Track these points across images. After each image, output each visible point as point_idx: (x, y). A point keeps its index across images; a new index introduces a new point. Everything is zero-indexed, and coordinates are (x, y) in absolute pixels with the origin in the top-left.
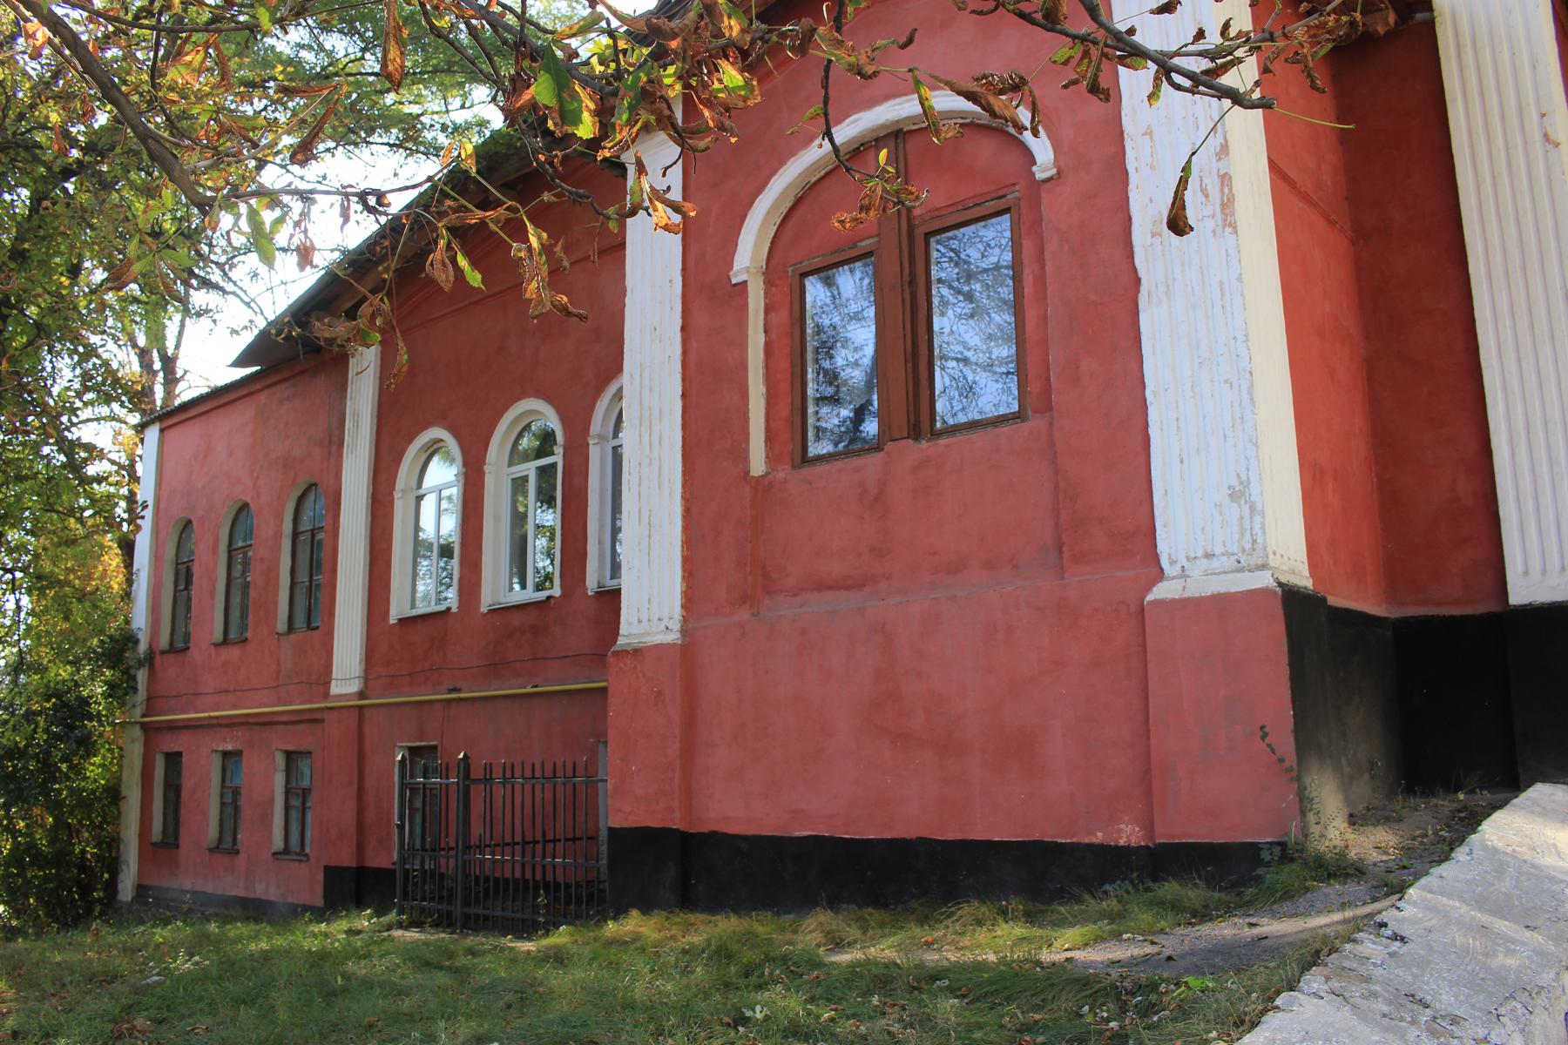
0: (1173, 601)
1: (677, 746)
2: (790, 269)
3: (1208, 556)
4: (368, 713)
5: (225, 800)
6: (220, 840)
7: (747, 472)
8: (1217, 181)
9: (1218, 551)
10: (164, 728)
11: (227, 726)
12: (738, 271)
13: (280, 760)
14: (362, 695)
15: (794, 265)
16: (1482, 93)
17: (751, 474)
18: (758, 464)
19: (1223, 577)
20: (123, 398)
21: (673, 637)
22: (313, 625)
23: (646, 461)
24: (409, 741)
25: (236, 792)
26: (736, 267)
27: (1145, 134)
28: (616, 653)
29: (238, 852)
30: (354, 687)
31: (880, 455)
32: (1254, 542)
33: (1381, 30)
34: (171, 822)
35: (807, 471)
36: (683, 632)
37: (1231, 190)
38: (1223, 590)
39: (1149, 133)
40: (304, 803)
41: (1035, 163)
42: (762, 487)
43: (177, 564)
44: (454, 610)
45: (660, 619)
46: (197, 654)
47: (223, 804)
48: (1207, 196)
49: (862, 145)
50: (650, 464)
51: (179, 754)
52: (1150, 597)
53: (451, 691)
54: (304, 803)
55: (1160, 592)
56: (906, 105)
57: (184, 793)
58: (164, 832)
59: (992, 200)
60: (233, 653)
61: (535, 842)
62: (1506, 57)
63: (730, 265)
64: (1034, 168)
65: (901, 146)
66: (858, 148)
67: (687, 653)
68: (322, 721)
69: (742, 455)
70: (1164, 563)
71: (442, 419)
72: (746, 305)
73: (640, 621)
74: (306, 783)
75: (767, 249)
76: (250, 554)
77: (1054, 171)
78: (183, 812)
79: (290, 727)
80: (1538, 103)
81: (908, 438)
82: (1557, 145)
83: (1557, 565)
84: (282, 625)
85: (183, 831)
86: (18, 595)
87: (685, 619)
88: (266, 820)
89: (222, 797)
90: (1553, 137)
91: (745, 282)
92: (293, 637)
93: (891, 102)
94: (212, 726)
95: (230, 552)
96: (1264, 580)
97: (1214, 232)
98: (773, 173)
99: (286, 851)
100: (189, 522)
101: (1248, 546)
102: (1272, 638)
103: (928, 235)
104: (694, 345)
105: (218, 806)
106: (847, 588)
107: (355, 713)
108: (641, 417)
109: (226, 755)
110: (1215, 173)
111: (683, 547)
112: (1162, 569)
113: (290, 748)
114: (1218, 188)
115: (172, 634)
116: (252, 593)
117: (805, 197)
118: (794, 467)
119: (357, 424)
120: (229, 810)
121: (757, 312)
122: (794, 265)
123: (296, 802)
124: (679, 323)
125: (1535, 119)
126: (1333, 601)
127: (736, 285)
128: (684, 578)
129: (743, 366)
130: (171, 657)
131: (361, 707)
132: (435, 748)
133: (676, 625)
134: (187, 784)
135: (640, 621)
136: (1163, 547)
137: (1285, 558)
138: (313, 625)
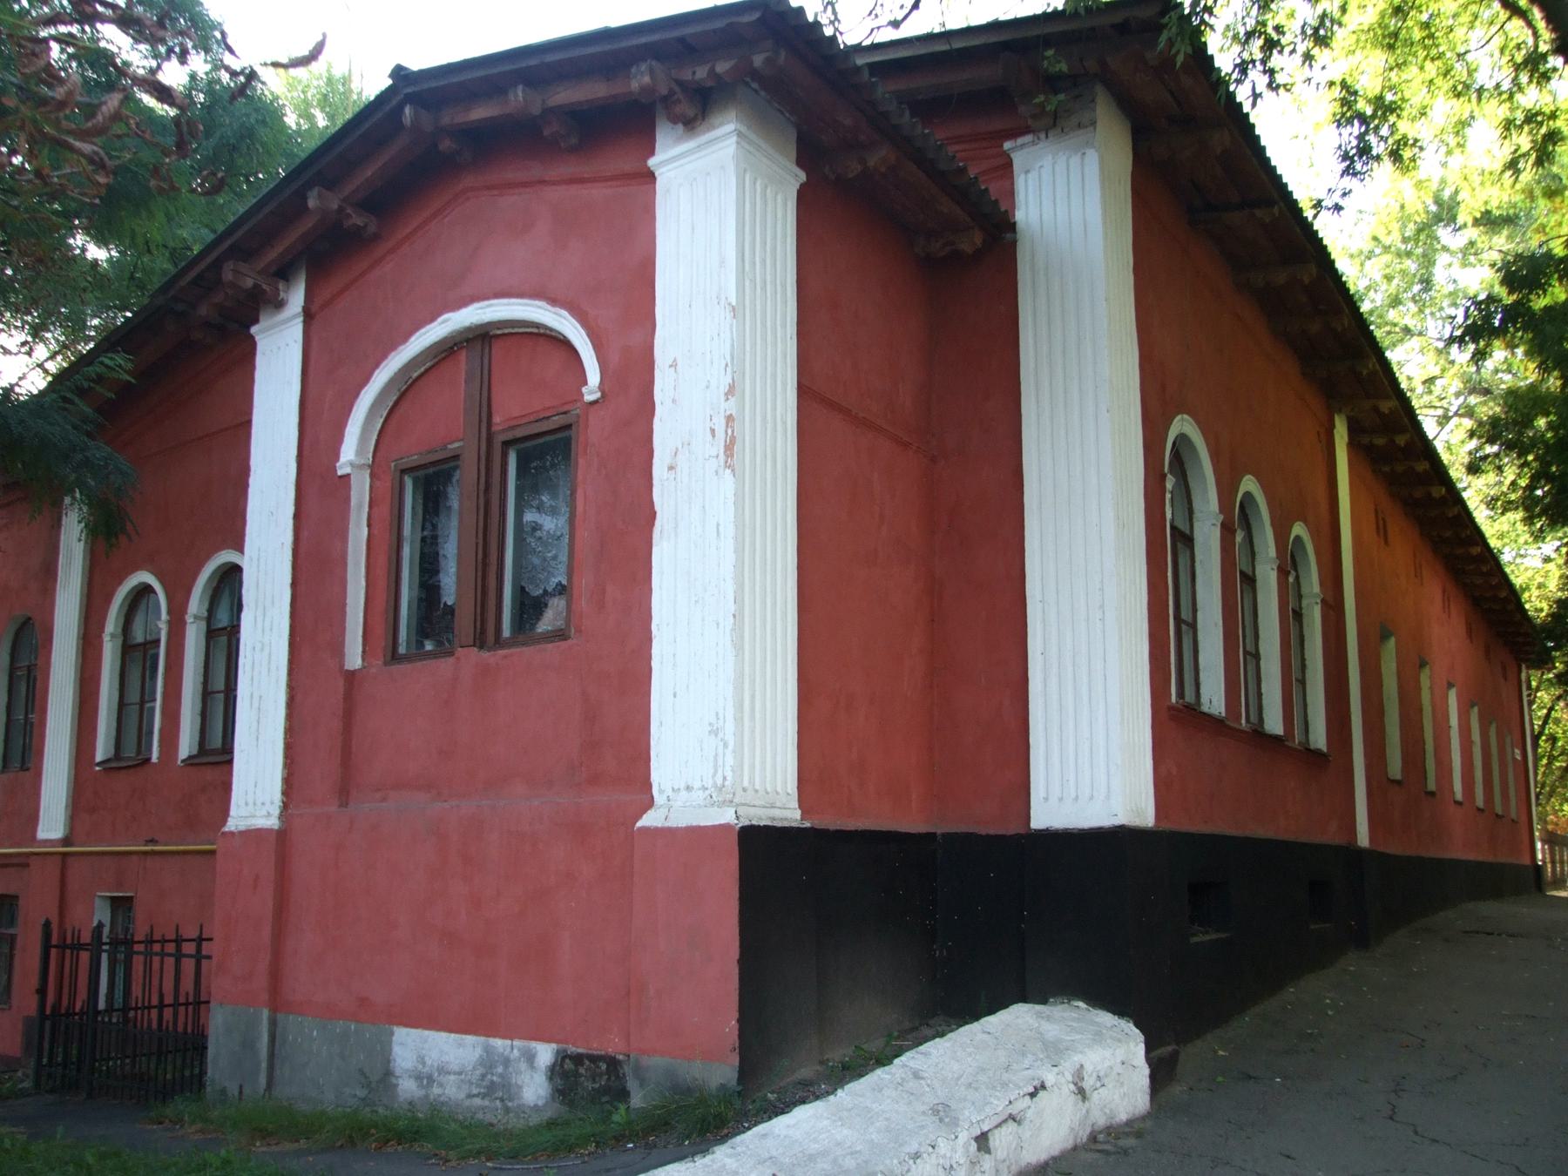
0: (657, 829)
2: (393, 464)
7: (342, 665)
8: (723, 421)
9: (697, 784)
12: (344, 464)
14: (66, 841)
15: (396, 460)
17: (346, 668)
18: (354, 658)
21: (273, 822)
23: (258, 646)
24: (109, 891)
27: (671, 366)
31: (451, 660)
36: (281, 816)
37: (733, 431)
39: (674, 365)
41: (585, 383)
42: (351, 676)
44: (155, 757)
45: (263, 804)
48: (714, 436)
49: (455, 344)
50: (262, 650)
52: (639, 824)
55: (649, 820)
56: (488, 310)
59: (558, 414)
61: (150, 1007)
63: (337, 457)
64: (584, 390)
65: (487, 351)
66: (452, 348)
67: (281, 841)
68: (28, 865)
69: (338, 649)
70: (655, 791)
72: (347, 499)
73: (247, 804)
75: (373, 442)
77: (598, 395)
81: (474, 645)
86: (1439, 247)
87: (285, 806)
93: (476, 305)
96: (727, 816)
97: (717, 472)
98: (377, 365)
102: (727, 867)
108: (257, 602)
110: (722, 414)
111: (286, 733)
112: (652, 797)
114: (723, 428)
117: (408, 387)
118: (386, 664)
121: (360, 506)
122: (396, 460)
127: (341, 477)
132: (130, 899)
133: (276, 812)
135: (247, 804)
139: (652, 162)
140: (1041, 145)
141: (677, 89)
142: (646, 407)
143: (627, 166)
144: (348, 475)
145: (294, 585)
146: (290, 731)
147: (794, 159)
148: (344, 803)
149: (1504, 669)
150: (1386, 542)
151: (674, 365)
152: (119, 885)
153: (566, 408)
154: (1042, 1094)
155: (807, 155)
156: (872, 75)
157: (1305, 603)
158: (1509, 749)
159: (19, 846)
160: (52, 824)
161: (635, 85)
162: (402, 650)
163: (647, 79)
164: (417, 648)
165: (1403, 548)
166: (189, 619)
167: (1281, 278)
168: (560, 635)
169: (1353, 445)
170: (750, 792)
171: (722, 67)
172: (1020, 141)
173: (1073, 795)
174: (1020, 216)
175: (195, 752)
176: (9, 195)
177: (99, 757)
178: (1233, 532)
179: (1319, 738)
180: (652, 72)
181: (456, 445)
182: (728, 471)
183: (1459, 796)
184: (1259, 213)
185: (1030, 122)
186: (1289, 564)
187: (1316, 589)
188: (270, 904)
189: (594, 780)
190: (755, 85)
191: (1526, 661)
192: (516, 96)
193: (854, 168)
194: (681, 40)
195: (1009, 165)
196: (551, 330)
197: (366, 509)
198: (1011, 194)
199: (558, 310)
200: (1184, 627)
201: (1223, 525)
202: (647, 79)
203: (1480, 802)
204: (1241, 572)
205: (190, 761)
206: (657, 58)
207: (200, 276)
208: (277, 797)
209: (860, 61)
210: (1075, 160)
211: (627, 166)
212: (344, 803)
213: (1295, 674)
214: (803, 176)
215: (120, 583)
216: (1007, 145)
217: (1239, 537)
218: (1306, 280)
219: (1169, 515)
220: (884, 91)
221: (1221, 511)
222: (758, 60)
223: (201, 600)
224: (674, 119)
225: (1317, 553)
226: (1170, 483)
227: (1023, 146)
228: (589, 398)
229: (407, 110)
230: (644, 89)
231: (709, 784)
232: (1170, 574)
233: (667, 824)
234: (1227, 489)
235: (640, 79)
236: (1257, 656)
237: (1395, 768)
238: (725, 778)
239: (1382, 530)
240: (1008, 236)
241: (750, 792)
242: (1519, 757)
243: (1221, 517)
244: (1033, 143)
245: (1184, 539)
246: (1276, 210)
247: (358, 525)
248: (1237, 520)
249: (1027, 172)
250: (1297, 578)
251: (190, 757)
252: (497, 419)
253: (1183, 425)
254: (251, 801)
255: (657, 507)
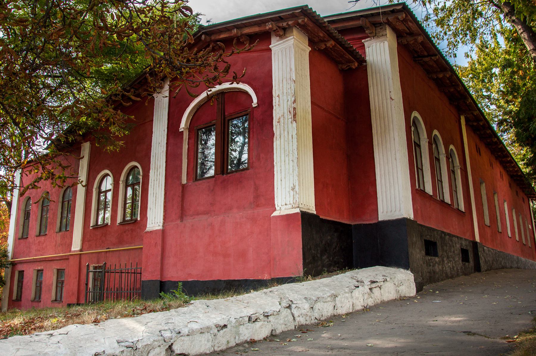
1: (160, 257)
3: (286, 205)
4: (82, 256)
5: (37, 285)
6: (35, 298)
9: (288, 203)
10: (19, 263)
11: (39, 261)
13: (55, 271)
14: (81, 250)
16: (377, 86)
18: (184, 181)
19: (289, 210)
20: (41, 86)
22: (67, 230)
23: (156, 180)
25: (41, 283)
26: (181, 127)
28: (146, 232)
29: (40, 301)
30: (78, 248)
32: (296, 201)
33: (354, 67)
34: (19, 293)
35: (197, 183)
36: (163, 226)
38: (288, 213)
40: (62, 285)
41: (253, 102)
42: (183, 186)
43: (25, 211)
44: (109, 224)
46: (30, 239)
47: (36, 286)
51: (23, 271)
52: (272, 215)
53: (107, 249)
54: (62, 285)
55: (275, 214)
57: (24, 283)
58: (17, 297)
60: (42, 239)
62: (382, 76)
67: (163, 232)
69: (179, 178)
70: (276, 206)
71: (108, 167)
72: (183, 137)
74: (63, 279)
76: (49, 208)
78: (23, 290)
79: (59, 261)
80: (389, 89)
82: (393, 100)
83: (398, 210)
84: (57, 229)
85: (23, 295)
87: (164, 223)
88: (50, 290)
89: (36, 284)
90: (392, 98)
91: (183, 131)
92: (60, 233)
94: (34, 262)
95: (42, 207)
96: (297, 210)
99: (56, 300)
100: (30, 198)
101: (295, 202)
103: (229, 120)
104: (169, 148)
105: (35, 287)
106: (205, 214)
107: (78, 257)
109: (38, 271)
113: (59, 268)
115: (23, 234)
116: (49, 220)
118: (193, 182)
119: (83, 168)
120: (39, 288)
123: (60, 285)
124: (166, 142)
125: (388, 92)
126: (321, 217)
128: (164, 211)
129: (181, 154)
130: (22, 240)
131: (80, 254)
133: (161, 225)
134: (25, 280)
136: (276, 203)
137: (306, 205)
138: (67, 230)
139: (270, 46)
140: (372, 40)
141: (277, 28)
142: (270, 107)
143: (264, 47)
144: (183, 131)
145: (166, 162)
146: (165, 202)
147: (307, 44)
148: (182, 221)
149: (523, 199)
150: (480, 155)
151: (278, 96)
152: (98, 263)
153: (246, 110)
154: (385, 282)
155: (311, 43)
156: (329, 23)
157: (455, 169)
158: (527, 224)
159: (65, 253)
160: (76, 245)
161: (267, 28)
162: (198, 178)
163: (271, 26)
164: (201, 177)
165: (486, 156)
166: (121, 182)
167: (441, 76)
168: (247, 169)
169: (467, 125)
170: (303, 205)
171: (290, 23)
172: (366, 40)
173: (390, 210)
174: (367, 58)
175: (122, 221)
176: (263, 25)
177: (91, 225)
178: (449, 159)
179: (462, 207)
180: (272, 24)
181: (214, 121)
182: (294, 122)
183: (510, 236)
184: (433, 58)
185: (369, 35)
186: (449, 156)
187: (458, 164)
188: (160, 250)
189: (258, 206)
190: (298, 27)
191: (530, 197)
192: (234, 31)
193: (323, 47)
194: (280, 17)
195: (364, 45)
196: (242, 89)
197: (187, 140)
198: (365, 53)
199: (244, 84)
200: (419, 170)
201: (429, 142)
202: (271, 26)
203: (517, 239)
204: (435, 157)
205: (121, 224)
206: (273, 21)
207: (141, 82)
208: (162, 221)
209: (325, 20)
210: (382, 41)
211: (264, 47)
212: (182, 221)
213: (454, 188)
214: (310, 49)
215: (98, 174)
216: (363, 41)
217: (434, 146)
218: (448, 76)
219: (413, 137)
220: (332, 27)
221: (428, 138)
222: (300, 21)
223: (124, 177)
224: (277, 35)
225: (458, 155)
226: (413, 129)
227: (367, 41)
228: (254, 106)
229: (203, 36)
230: (270, 29)
231: (292, 203)
232: (414, 153)
233: (280, 214)
234: (429, 134)
235: (269, 26)
236: (441, 182)
237: (487, 222)
238: (296, 201)
239: (478, 151)
240: (365, 64)
241: (303, 205)
242: (530, 228)
243: (428, 140)
244: (370, 40)
245: (418, 145)
246: (437, 57)
247: (185, 145)
248: (432, 142)
249: (369, 47)
250: (452, 160)
251: (120, 223)
252: (226, 114)
253: (415, 114)
254: (153, 222)
255: (275, 132)
